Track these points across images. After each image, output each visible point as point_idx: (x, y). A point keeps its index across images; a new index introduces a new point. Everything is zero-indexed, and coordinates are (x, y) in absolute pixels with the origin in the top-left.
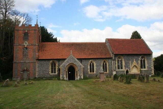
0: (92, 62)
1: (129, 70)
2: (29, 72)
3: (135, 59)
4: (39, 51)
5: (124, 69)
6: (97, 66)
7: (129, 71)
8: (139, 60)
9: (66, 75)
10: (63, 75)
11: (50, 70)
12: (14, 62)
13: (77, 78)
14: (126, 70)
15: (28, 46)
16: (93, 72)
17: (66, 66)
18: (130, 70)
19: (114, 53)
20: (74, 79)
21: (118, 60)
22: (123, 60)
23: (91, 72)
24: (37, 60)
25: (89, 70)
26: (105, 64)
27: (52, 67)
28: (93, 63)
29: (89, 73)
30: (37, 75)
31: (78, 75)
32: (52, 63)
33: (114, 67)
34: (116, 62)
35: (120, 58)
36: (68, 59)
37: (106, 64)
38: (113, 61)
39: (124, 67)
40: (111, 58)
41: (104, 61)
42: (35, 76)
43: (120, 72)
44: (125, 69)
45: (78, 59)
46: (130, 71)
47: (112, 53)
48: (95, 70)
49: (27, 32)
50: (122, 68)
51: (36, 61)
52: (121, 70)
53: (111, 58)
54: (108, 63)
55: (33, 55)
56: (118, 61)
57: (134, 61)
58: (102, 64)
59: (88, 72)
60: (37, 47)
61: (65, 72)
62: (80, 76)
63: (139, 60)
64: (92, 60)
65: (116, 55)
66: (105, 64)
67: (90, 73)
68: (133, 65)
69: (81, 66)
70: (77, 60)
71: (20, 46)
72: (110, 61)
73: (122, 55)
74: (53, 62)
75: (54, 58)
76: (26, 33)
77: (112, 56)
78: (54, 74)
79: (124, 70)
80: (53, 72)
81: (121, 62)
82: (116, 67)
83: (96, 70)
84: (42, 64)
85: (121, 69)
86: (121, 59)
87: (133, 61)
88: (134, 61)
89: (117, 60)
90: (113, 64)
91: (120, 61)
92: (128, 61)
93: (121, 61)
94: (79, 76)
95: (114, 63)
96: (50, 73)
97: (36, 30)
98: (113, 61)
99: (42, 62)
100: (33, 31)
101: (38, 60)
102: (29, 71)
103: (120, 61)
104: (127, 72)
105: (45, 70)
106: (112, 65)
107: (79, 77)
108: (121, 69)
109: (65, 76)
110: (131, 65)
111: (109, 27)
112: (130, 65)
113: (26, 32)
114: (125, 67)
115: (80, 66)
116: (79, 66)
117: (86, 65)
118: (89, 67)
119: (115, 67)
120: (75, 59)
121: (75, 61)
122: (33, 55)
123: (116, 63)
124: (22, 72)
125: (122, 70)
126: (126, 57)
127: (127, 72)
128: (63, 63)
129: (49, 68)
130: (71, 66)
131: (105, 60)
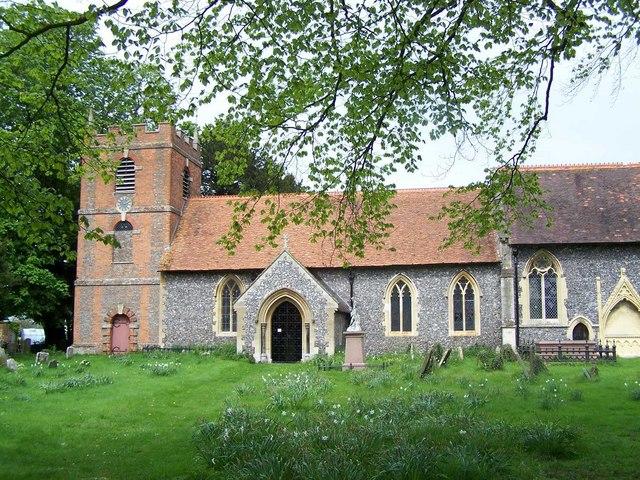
0: (401, 283)
1: (589, 325)
2: (132, 326)
3: (623, 270)
5: (565, 320)
7: (591, 330)
8: (315, 287)
9: (263, 338)
11: (218, 318)
13: (309, 352)
15: (134, 216)
16: (408, 328)
17: (260, 302)
18: (596, 321)
19: (510, 242)
20: (299, 357)
21: (535, 271)
22: (560, 272)
23: (395, 327)
25: (387, 322)
26: (464, 293)
27: (223, 304)
29: (389, 333)
31: (312, 341)
32: (226, 288)
33: (508, 307)
34: (524, 284)
35: (543, 264)
36: (269, 271)
37: (470, 294)
39: (562, 310)
40: (494, 266)
41: (463, 281)
42: (157, 341)
43: (541, 332)
46: (596, 328)
47: (503, 242)
48: (415, 319)
49: (128, 159)
50: (552, 313)
53: (494, 266)
54: (482, 287)
55: (153, 252)
56: (534, 276)
57: (624, 278)
58: (451, 294)
59: (383, 329)
60: (167, 217)
61: (258, 328)
62: (321, 346)
63: (315, 287)
65: (520, 251)
66: (464, 293)
68: (613, 300)
69: (323, 303)
70: (308, 276)
72: (490, 278)
73: (557, 249)
74: (231, 282)
75: (234, 267)
76: (125, 159)
77: (503, 254)
81: (552, 287)
82: (518, 308)
87: (616, 280)
88: (624, 278)
89: (525, 273)
90: (503, 294)
91: (543, 279)
93: (551, 276)
94: (317, 345)
95: (507, 289)
96: (217, 328)
97: (163, 148)
99: (183, 285)
100: (154, 151)
101: (169, 275)
103: (543, 279)
104: (581, 331)
105: (194, 318)
106: (498, 296)
107: (315, 351)
109: (256, 344)
110: (605, 298)
112: (599, 296)
113: (126, 156)
116: (318, 304)
117: (374, 296)
118: (387, 307)
119: (513, 306)
120: (303, 271)
121: (303, 282)
122: (153, 252)
123: (517, 289)
125: (552, 322)
126: (576, 263)
127: (581, 331)
130: (283, 304)
131: (463, 273)
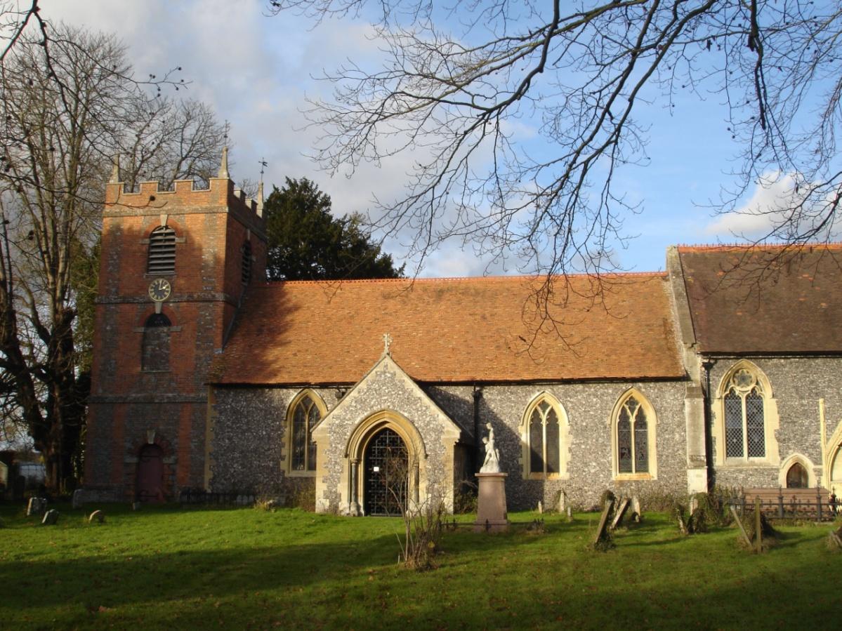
4: (228, 338)
6: (578, 431)
10: (332, 481)
12: (93, 395)
14: (788, 463)
16: (643, 466)
21: (732, 391)
24: (215, 386)
26: (632, 420)
28: (552, 412)
30: (208, 476)
36: (362, 386)
38: (687, 402)
39: (771, 444)
44: (783, 455)
49: (167, 227)
51: (205, 394)
52: (756, 459)
64: (548, 395)
66: (632, 420)
70: (419, 392)
71: (126, 307)
72: (670, 393)
76: (160, 228)
78: (633, 476)
79: (776, 464)
80: (302, 462)
83: (569, 456)
84: (241, 414)
85: (750, 454)
86: (750, 388)
90: (687, 421)
92: (802, 398)
102: (172, 452)
105: (255, 451)
106: (681, 424)
108: (750, 454)
109: (343, 489)
111: (337, 211)
114: (781, 439)
115: (434, 430)
121: (410, 400)
124: (135, 460)
127: (797, 475)
129: (280, 436)
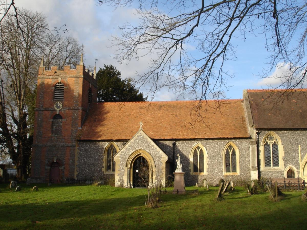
4: (83, 123)
5: (282, 168)
6: (211, 157)
10: (121, 175)
12: (34, 144)
14: (287, 169)
16: (234, 170)
21: (267, 142)
24: (78, 141)
26: (231, 153)
28: (201, 150)
30: (76, 173)
36: (132, 141)
38: (250, 146)
39: (281, 162)
44: (285, 166)
45: (154, 140)
49: (61, 83)
51: (75, 143)
52: (276, 167)
64: (200, 144)
66: (231, 153)
67: (194, 174)
71: (46, 112)
72: (244, 143)
78: (231, 173)
79: (283, 169)
80: (110, 168)
83: (207, 166)
84: (88, 151)
85: (273, 166)
90: (251, 153)
92: (292, 145)
98: (250, 146)
102: (63, 165)
105: (93, 164)
106: (248, 155)
108: (273, 166)
109: (125, 178)
111: (123, 77)
114: (285, 160)
115: (158, 157)
121: (149, 146)
124: (49, 168)
127: (291, 173)
128: (122, 150)
129: (102, 159)
